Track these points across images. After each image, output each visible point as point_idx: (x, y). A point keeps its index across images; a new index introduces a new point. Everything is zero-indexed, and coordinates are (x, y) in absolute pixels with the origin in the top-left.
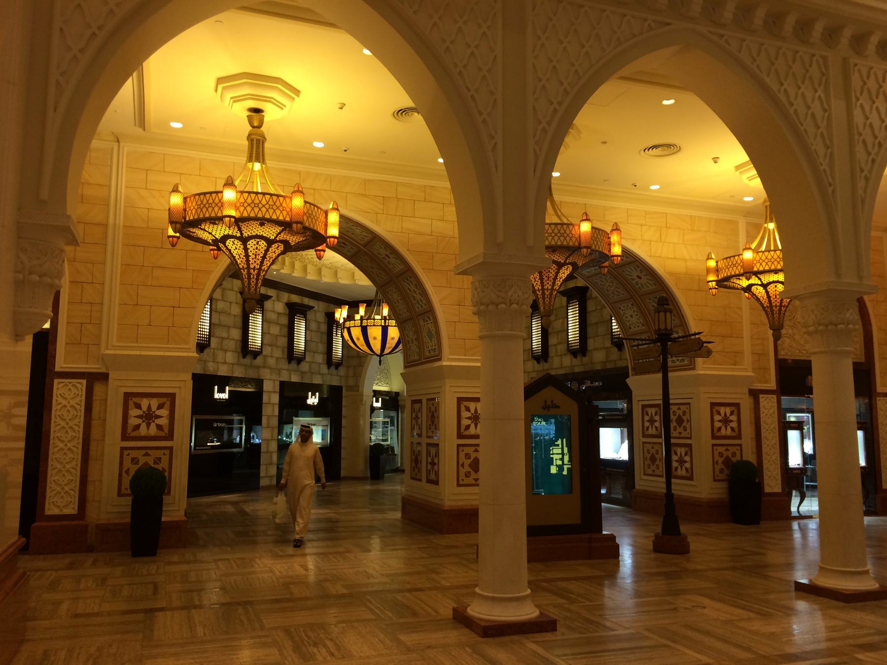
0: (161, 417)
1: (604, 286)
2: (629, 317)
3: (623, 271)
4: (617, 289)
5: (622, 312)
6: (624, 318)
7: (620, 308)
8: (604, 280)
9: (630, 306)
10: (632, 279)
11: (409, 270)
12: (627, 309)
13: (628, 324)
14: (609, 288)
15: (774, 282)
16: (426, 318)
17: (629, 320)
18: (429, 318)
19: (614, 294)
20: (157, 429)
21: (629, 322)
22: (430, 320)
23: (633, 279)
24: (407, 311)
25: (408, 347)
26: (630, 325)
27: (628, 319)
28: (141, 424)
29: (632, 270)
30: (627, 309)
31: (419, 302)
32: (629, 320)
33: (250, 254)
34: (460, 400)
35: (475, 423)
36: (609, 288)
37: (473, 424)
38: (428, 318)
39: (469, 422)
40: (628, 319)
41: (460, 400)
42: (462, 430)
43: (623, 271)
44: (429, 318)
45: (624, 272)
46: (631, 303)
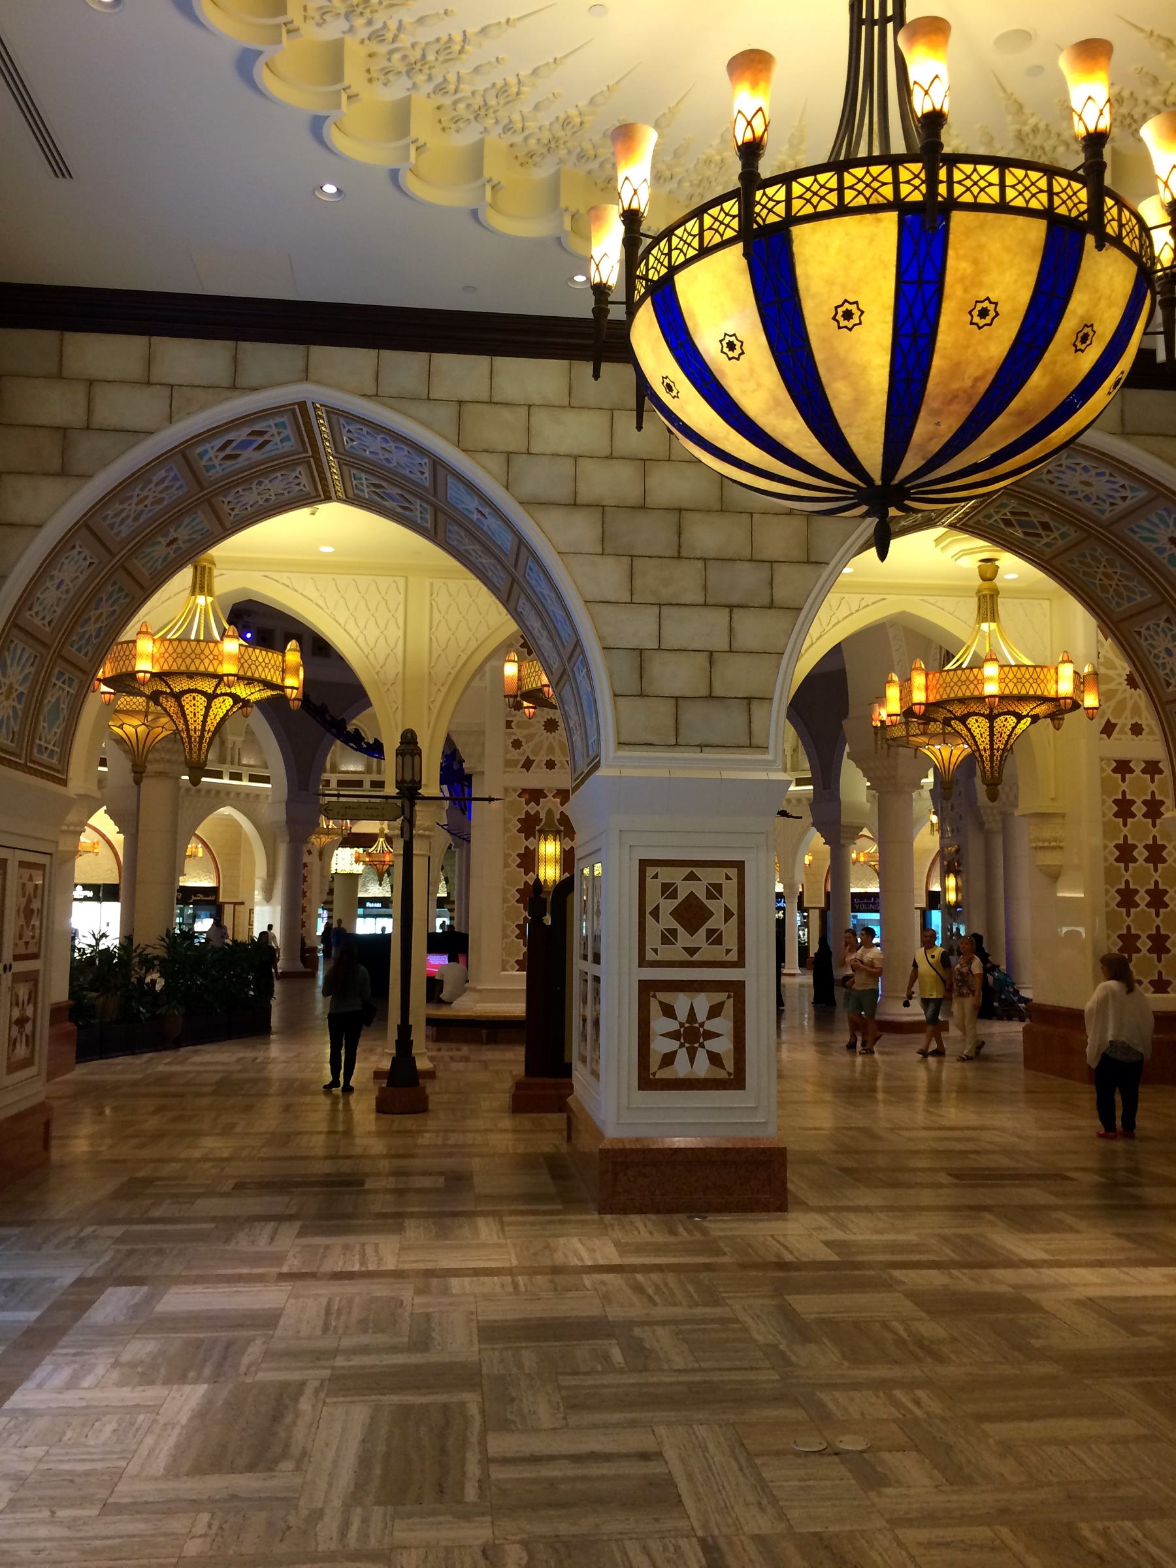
0: (718, 1035)
1: (1095, 578)
2: (1163, 654)
3: (1131, 530)
4: (1125, 583)
5: (1145, 644)
6: (1151, 658)
7: (1139, 633)
8: (1089, 560)
9: (1163, 624)
10: (1157, 549)
11: (225, 529)
12: (1157, 632)
13: (1161, 673)
14: (1106, 582)
15: (190, 691)
16: (204, 462)
17: (1164, 664)
18: (201, 455)
19: (1120, 595)
20: (665, 1055)
21: (1164, 668)
22: (206, 451)
23: (1161, 550)
24: (74, 547)
25: (28, 685)
26: (1167, 674)
27: (1160, 662)
28: (676, 1052)
29: (1155, 525)
30: (1157, 632)
31: (167, 488)
32: (1164, 664)
33: (187, 712)
34: (737, 1081)
35: (696, 1021)
36: (1106, 582)
37: (699, 1021)
38: (201, 458)
39: (682, 1013)
40: (1160, 662)
41: (737, 1081)
42: (729, 1006)
43: (1131, 530)
44: (201, 455)
45: (1135, 533)
46: (1165, 617)
